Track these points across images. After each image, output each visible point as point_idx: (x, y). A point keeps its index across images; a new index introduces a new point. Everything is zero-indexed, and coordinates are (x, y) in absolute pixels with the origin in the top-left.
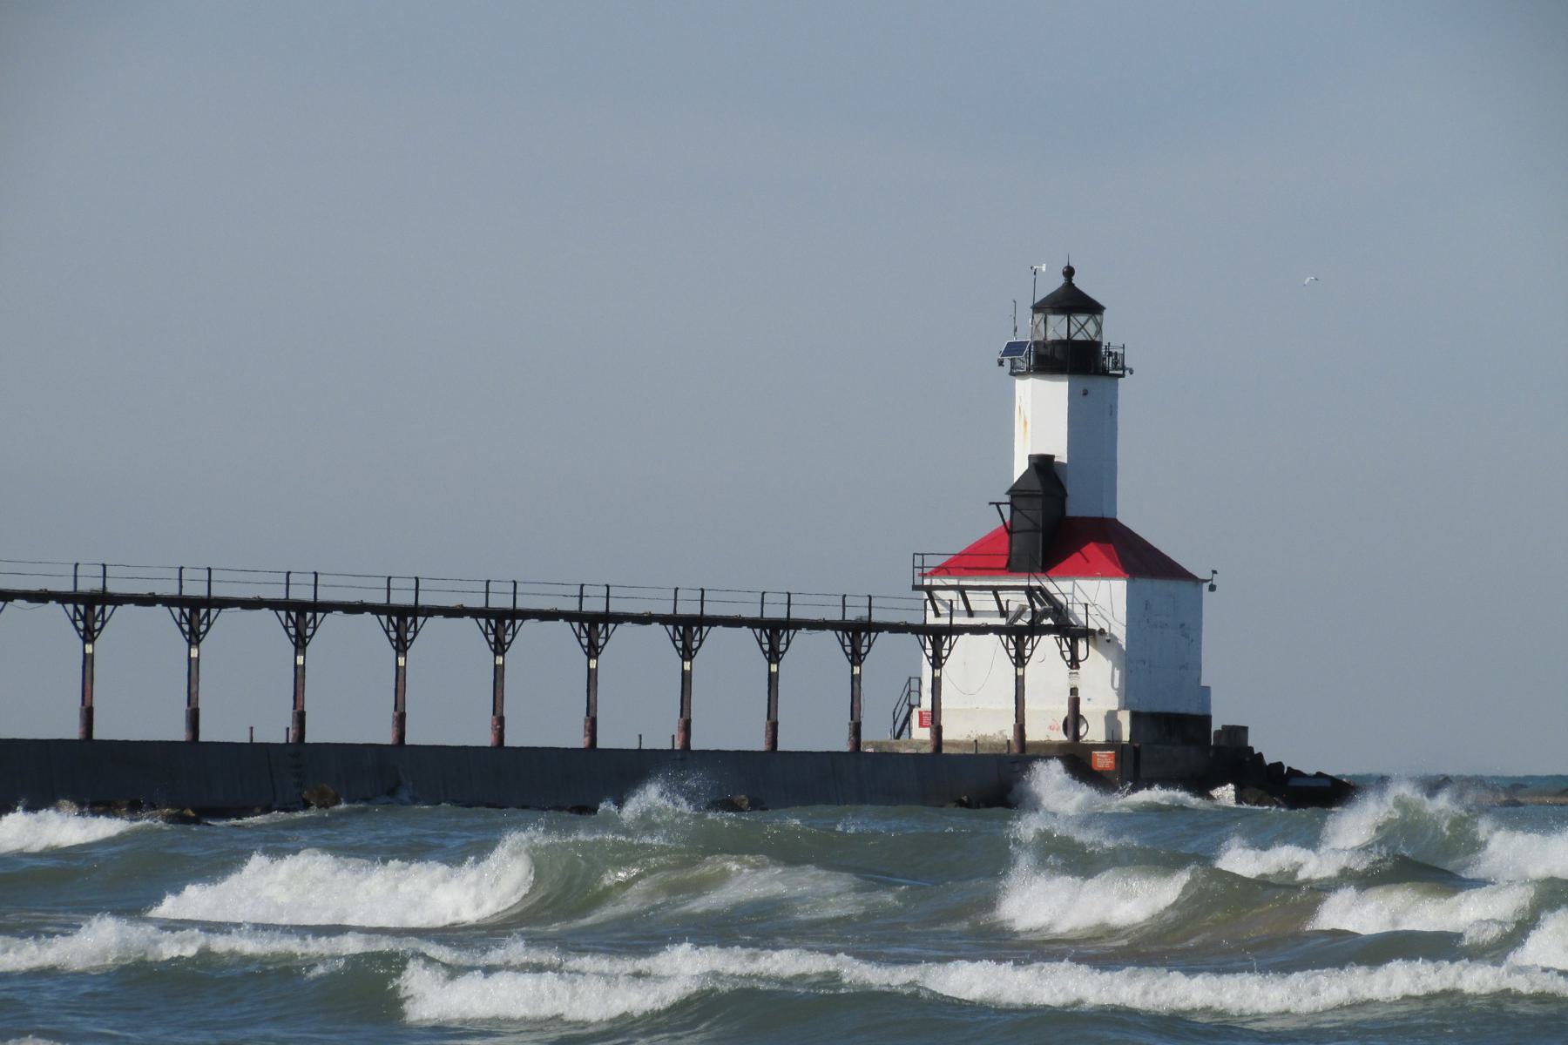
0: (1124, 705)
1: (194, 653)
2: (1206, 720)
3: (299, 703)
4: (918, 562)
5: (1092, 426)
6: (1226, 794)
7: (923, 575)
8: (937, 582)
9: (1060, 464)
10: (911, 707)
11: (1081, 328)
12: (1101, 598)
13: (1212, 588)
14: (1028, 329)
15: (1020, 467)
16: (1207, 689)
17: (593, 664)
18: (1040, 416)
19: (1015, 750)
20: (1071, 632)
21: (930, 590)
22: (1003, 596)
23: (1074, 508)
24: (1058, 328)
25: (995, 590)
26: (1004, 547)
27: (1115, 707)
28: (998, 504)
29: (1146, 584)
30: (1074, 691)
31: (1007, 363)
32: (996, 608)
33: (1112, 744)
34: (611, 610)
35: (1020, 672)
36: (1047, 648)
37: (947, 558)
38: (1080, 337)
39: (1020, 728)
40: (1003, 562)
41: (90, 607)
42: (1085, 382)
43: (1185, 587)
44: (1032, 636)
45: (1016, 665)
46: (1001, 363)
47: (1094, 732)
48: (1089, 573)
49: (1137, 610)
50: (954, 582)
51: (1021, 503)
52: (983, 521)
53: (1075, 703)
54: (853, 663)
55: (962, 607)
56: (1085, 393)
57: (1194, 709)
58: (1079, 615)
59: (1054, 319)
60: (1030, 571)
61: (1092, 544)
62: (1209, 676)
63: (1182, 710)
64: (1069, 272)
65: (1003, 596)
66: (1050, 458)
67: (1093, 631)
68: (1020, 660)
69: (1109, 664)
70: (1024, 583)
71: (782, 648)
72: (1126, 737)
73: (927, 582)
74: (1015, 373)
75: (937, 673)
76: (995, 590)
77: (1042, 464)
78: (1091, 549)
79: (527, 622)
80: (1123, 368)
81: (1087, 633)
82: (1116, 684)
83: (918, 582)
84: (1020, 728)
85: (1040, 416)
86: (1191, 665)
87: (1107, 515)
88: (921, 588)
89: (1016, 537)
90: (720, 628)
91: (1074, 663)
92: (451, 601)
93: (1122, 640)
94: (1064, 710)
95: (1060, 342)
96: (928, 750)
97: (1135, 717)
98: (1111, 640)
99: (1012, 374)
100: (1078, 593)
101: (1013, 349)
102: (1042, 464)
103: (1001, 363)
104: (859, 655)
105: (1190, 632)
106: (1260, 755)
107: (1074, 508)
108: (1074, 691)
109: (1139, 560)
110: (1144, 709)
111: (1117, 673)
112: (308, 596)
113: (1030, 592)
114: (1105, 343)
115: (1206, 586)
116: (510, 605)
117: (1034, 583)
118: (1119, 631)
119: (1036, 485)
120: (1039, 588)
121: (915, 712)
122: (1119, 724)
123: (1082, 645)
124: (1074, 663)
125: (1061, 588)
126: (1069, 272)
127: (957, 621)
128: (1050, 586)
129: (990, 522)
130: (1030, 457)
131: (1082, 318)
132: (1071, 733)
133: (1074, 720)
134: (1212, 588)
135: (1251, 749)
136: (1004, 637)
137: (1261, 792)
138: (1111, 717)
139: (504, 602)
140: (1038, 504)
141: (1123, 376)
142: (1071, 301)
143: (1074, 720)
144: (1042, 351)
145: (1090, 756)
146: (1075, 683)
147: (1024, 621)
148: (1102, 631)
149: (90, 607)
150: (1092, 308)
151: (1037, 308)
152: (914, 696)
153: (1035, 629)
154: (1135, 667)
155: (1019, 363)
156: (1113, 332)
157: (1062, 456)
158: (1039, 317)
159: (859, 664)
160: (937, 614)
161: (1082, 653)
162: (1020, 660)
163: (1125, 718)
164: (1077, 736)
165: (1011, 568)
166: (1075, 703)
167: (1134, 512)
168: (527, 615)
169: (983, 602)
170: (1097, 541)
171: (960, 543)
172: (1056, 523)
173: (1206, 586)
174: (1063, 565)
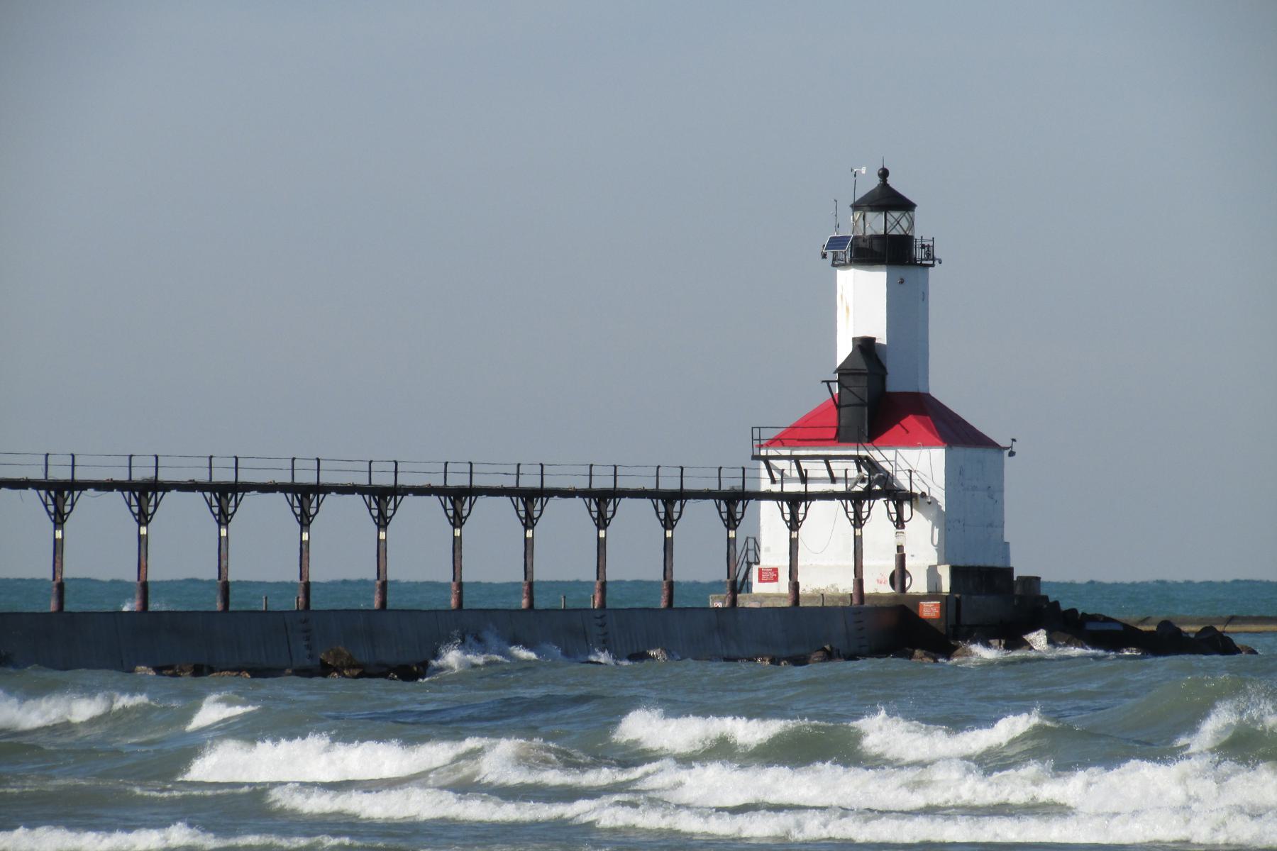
0: (943, 560)
1: (382, 535)
2: (1011, 570)
3: (668, 574)
4: (756, 436)
5: (906, 309)
6: (1038, 639)
7: (760, 447)
8: (772, 452)
9: (880, 345)
10: (749, 565)
11: (895, 223)
12: (922, 465)
13: (1012, 454)
14: (853, 225)
15: (844, 350)
16: (1007, 544)
17: (602, 534)
18: (861, 304)
19: (855, 602)
20: (899, 497)
21: (766, 459)
22: (833, 465)
23: (895, 384)
24: (875, 224)
25: (827, 459)
26: (833, 419)
27: (935, 562)
28: (828, 382)
29: (960, 452)
30: (900, 548)
31: (830, 254)
32: (826, 474)
33: (933, 594)
34: (545, 485)
35: (858, 532)
36: (879, 509)
37: (779, 431)
38: (894, 232)
39: (859, 582)
40: (832, 434)
41: (60, 494)
42: (901, 272)
43: (988, 454)
44: (155, 492)
45: (855, 526)
46: (824, 256)
47: (918, 585)
48: (911, 443)
49: (954, 475)
50: (786, 452)
51: (848, 381)
52: (813, 394)
53: (901, 559)
54: (526, 527)
55: (796, 474)
56: (902, 282)
57: (998, 563)
58: (903, 480)
59: (870, 216)
60: (857, 441)
61: (910, 417)
62: (1010, 534)
63: (990, 564)
64: (884, 174)
65: (833, 465)
66: (873, 340)
67: (916, 495)
68: (858, 522)
69: (930, 523)
70: (854, 453)
71: (312, 511)
72: (946, 587)
73: (763, 453)
74: (837, 263)
75: (794, 535)
76: (827, 459)
77: (865, 346)
78: (910, 421)
79: (479, 499)
80: (934, 259)
81: (911, 497)
82: (936, 542)
83: (756, 453)
84: (859, 582)
85: (861, 304)
86: (994, 523)
87: (922, 390)
88: (758, 458)
89: (843, 410)
90: (174, 492)
91: (900, 523)
92: (103, 476)
93: (942, 502)
94: (891, 565)
95: (877, 237)
96: (786, 603)
97: (956, 572)
98: (933, 502)
99: (833, 265)
100: (899, 460)
101: (836, 243)
102: (865, 346)
103: (824, 256)
104: (532, 519)
105: (994, 493)
106: (1056, 603)
107: (895, 384)
108: (900, 548)
109: (953, 431)
110: (961, 563)
111: (936, 531)
112: (312, 479)
113: (859, 461)
114: (917, 236)
115: (1006, 452)
116: (467, 483)
117: (863, 453)
118: (939, 494)
119: (861, 365)
120: (867, 458)
121: (755, 569)
122: (939, 577)
123: (907, 507)
124: (900, 523)
125: (885, 456)
126: (884, 174)
127: (812, 488)
128: (876, 455)
129: (820, 397)
130: (854, 339)
131: (896, 214)
132: (898, 586)
133: (900, 575)
134: (1012, 454)
135: (1046, 598)
136: (367, 497)
137: (1068, 636)
138: (932, 571)
139: (673, 485)
140: (863, 381)
141: (933, 265)
142: (887, 199)
143: (900, 575)
144: (862, 244)
145: (917, 606)
146: (900, 541)
147: (860, 487)
148: (923, 495)
149: (60, 494)
150: (905, 205)
151: (856, 207)
152: (751, 554)
153: (869, 494)
154: (952, 528)
155: (841, 256)
156: (923, 227)
157: (882, 339)
158: (858, 215)
159: (735, 529)
160: (773, 481)
161: (906, 516)
162: (858, 522)
163: (945, 572)
164: (903, 589)
165: (841, 437)
166: (901, 559)
167: (944, 386)
168: (84, 486)
169: (816, 469)
170: (915, 413)
171: (791, 417)
172: (877, 399)
173: (1006, 452)
174: (887, 434)
